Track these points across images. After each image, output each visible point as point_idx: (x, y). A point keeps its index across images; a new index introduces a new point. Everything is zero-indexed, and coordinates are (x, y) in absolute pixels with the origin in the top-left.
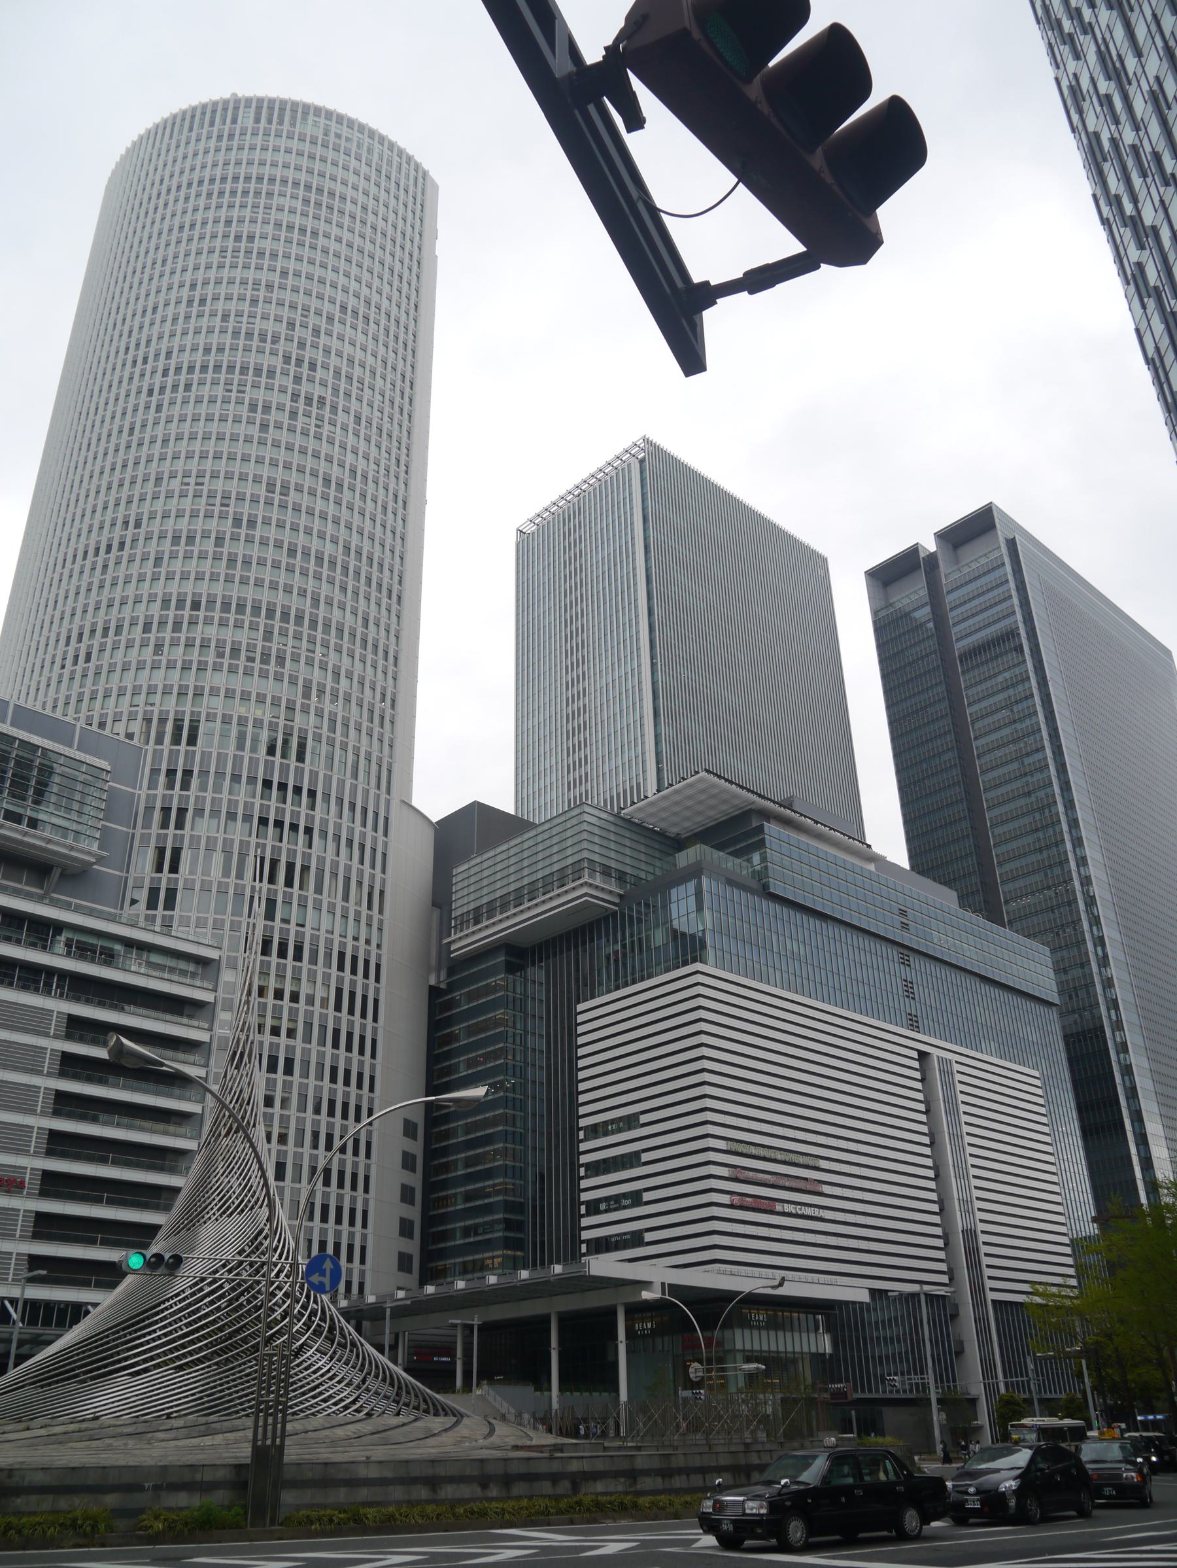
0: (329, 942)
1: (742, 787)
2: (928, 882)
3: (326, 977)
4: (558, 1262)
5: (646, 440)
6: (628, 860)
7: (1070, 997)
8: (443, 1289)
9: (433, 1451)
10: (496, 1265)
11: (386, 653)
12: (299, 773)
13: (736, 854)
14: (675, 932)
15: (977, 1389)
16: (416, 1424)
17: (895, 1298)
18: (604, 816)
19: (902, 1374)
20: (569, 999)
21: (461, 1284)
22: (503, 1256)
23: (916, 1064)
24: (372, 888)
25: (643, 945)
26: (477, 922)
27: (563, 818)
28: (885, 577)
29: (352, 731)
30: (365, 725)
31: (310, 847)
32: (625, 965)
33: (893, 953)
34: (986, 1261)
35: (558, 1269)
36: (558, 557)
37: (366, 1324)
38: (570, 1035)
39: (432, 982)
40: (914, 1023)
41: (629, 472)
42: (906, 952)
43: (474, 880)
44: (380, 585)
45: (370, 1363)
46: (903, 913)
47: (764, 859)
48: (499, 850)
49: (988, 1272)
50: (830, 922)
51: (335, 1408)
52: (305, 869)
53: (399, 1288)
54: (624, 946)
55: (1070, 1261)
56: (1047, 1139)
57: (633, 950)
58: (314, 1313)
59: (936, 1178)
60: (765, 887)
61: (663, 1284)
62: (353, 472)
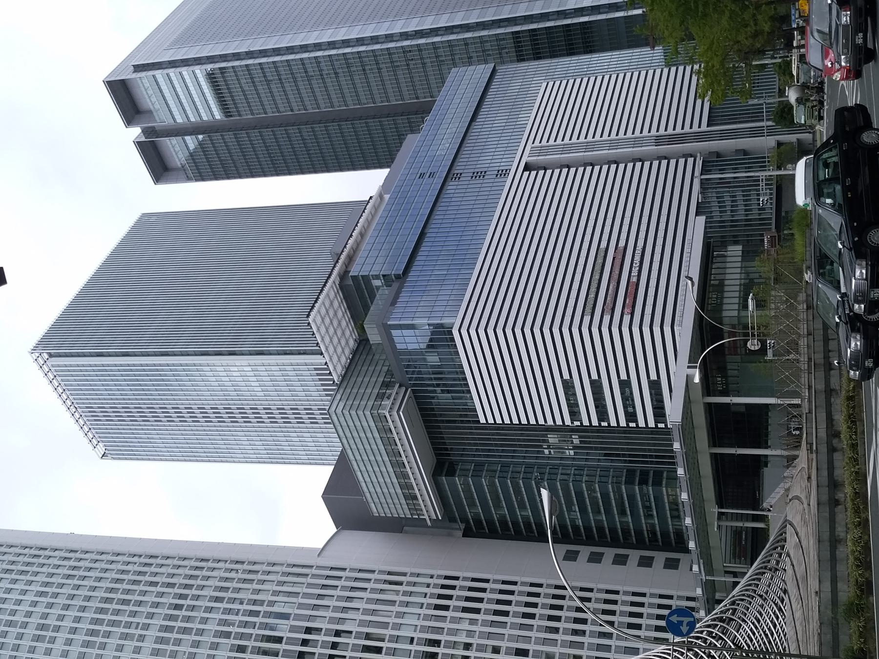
0: (427, 617)
1: (322, 291)
2: (400, 155)
3: (454, 620)
4: (672, 445)
5: (35, 349)
6: (374, 379)
7: (489, 55)
8: (691, 536)
9: (811, 542)
10: (674, 493)
11: (197, 568)
12: (291, 641)
13: (372, 297)
14: (429, 346)
15: (770, 142)
16: (792, 556)
17: (703, 198)
18: (338, 397)
19: (758, 195)
20: (477, 428)
21: (688, 521)
22: (666, 487)
23: (534, 173)
24: (385, 582)
25: (438, 371)
26: (415, 498)
27: (339, 428)
28: (160, 168)
29: (259, 597)
30: (255, 586)
31: (351, 632)
32: (452, 386)
33: (451, 186)
34: (679, 130)
35: (676, 446)
36: (121, 427)
37: (718, 596)
38: (503, 429)
39: (460, 533)
40: (503, 173)
41: (59, 366)
42: (451, 176)
43: (379, 491)
44: (140, 573)
45: (747, 590)
46: (422, 176)
47: (377, 277)
48: (361, 479)
49: (687, 129)
50: (426, 231)
51: (780, 618)
52: (368, 636)
53: (691, 570)
54: (438, 385)
55: (681, 68)
56: (592, 79)
57: (441, 379)
58: (710, 634)
59: (617, 163)
60: (398, 277)
61: (689, 367)
62: (42, 594)
